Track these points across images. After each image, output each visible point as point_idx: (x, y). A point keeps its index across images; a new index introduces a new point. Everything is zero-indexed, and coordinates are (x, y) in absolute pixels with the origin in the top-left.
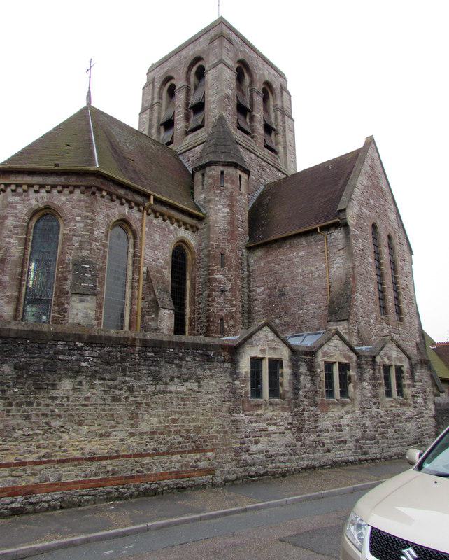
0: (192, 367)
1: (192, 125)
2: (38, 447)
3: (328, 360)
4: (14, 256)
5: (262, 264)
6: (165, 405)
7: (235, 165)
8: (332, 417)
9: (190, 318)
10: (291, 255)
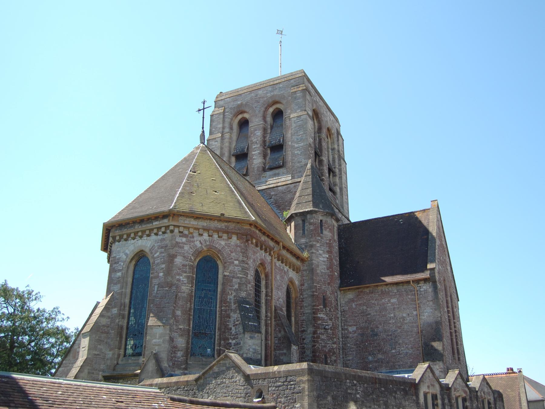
5: (354, 306)
10: (383, 301)
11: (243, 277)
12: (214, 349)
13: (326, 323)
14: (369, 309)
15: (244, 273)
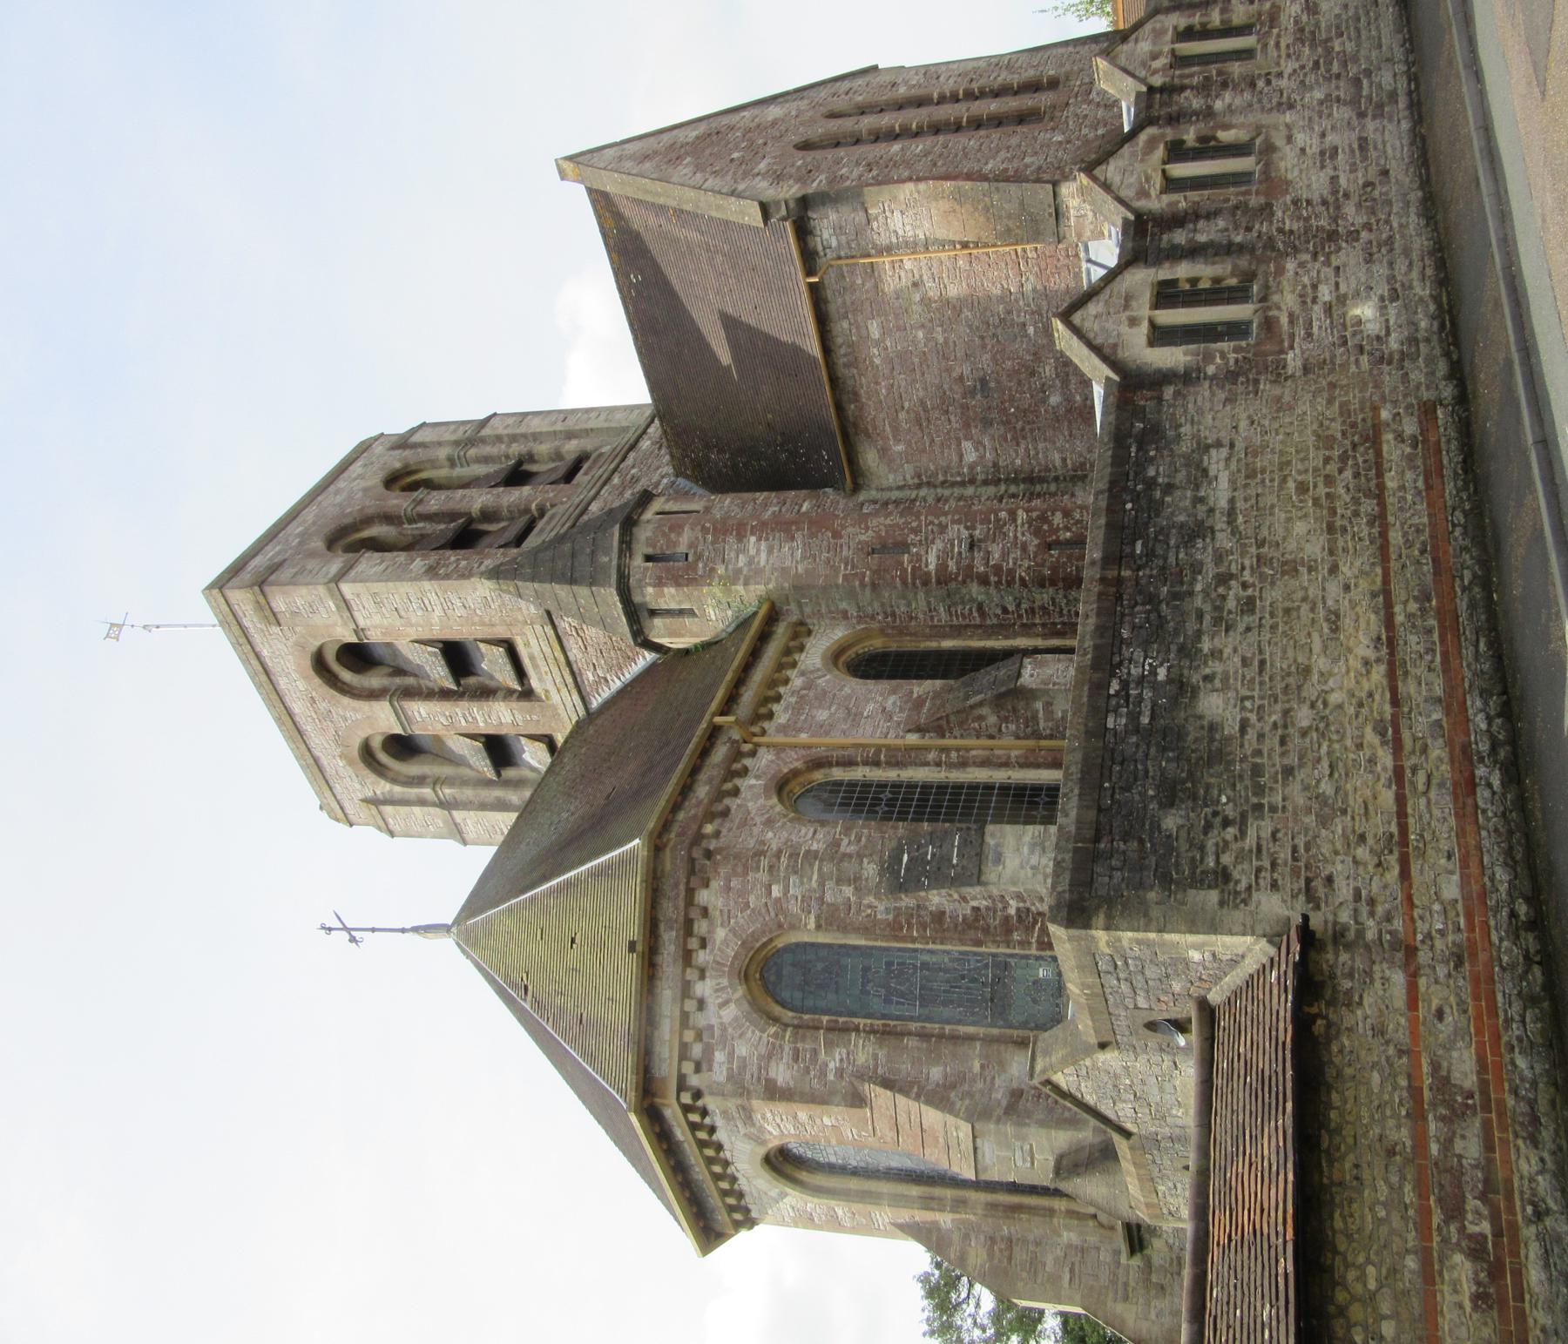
0: (1172, 463)
1: (507, 677)
2: (1360, 746)
3: (1158, 186)
4: (875, 1057)
5: (900, 448)
6: (1265, 509)
7: (630, 525)
8: (1301, 171)
9: (1045, 636)
10: (877, 361)
11: (820, 869)
12: (1038, 958)
13: (953, 545)
14: (906, 405)
15: (807, 867)
